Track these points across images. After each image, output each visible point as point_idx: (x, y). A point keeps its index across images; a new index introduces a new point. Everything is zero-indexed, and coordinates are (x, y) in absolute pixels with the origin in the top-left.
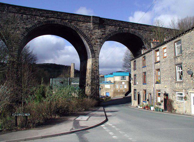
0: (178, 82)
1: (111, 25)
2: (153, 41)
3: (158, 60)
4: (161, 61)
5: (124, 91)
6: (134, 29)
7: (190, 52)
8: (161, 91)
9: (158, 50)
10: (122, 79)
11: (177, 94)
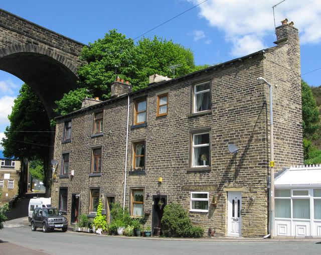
0: (195, 171)
1: (9, 29)
2: (118, 81)
3: (138, 122)
4: (150, 123)
5: (7, 195)
6: (62, 50)
7: (233, 108)
8: (146, 191)
9: (165, 96)
10: (5, 167)
11: (191, 197)
